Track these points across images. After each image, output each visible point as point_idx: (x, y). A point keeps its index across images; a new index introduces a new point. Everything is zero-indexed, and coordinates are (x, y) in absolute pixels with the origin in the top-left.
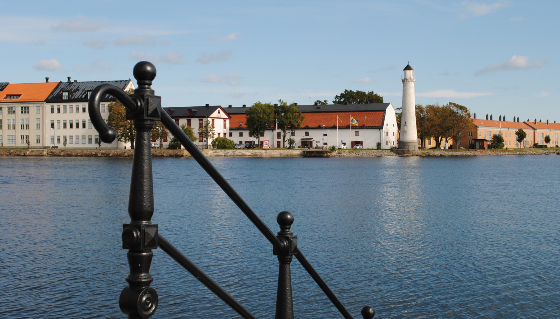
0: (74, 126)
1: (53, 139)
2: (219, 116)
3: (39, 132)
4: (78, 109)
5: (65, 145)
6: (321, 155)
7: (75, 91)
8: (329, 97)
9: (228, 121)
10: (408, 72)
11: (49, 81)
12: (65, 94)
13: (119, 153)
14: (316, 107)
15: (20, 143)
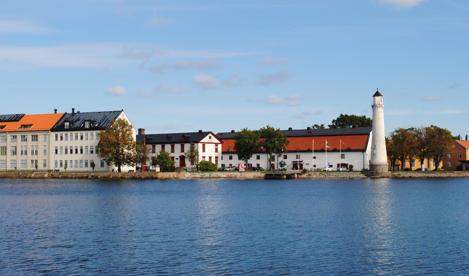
0: (74, 151)
1: (56, 163)
2: (210, 141)
3: (46, 157)
4: (77, 137)
5: (65, 169)
6: (280, 177)
7: (76, 121)
8: (327, 123)
9: (220, 146)
10: (377, 98)
11: (58, 112)
12: (67, 124)
13: (105, 175)
14: (308, 131)
15: (30, 167)
